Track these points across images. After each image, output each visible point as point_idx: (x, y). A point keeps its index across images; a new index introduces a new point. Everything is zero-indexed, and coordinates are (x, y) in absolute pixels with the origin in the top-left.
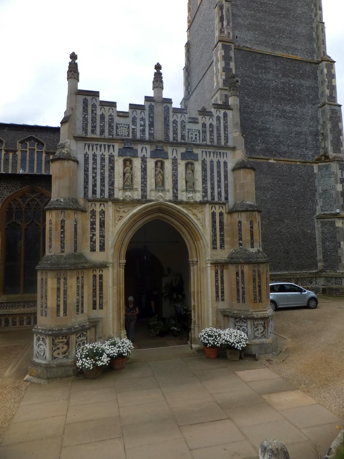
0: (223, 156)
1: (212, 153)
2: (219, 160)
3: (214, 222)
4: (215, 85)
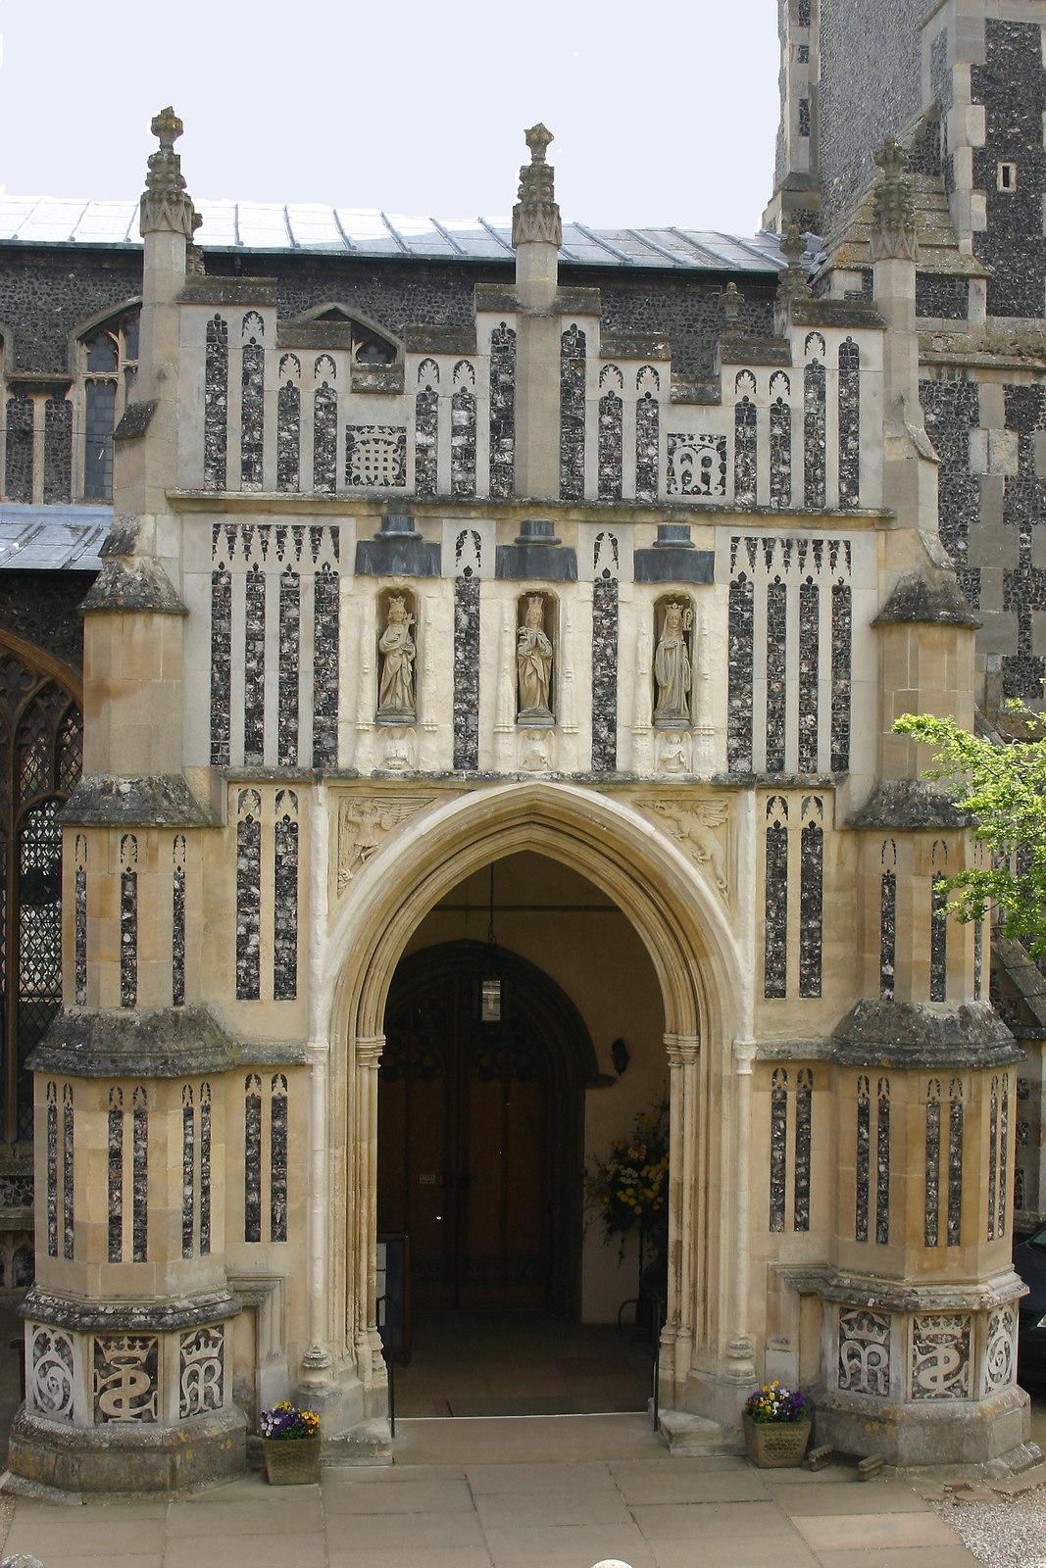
0: (834, 556)
1: (778, 545)
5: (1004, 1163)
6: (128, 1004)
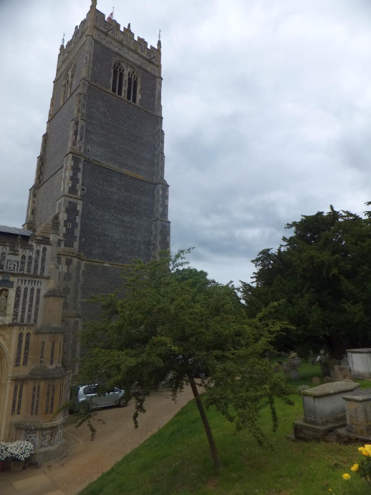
0: (38, 283)
1: (27, 281)
2: (33, 287)
3: (20, 342)
4: (62, 189)
5: (62, 396)
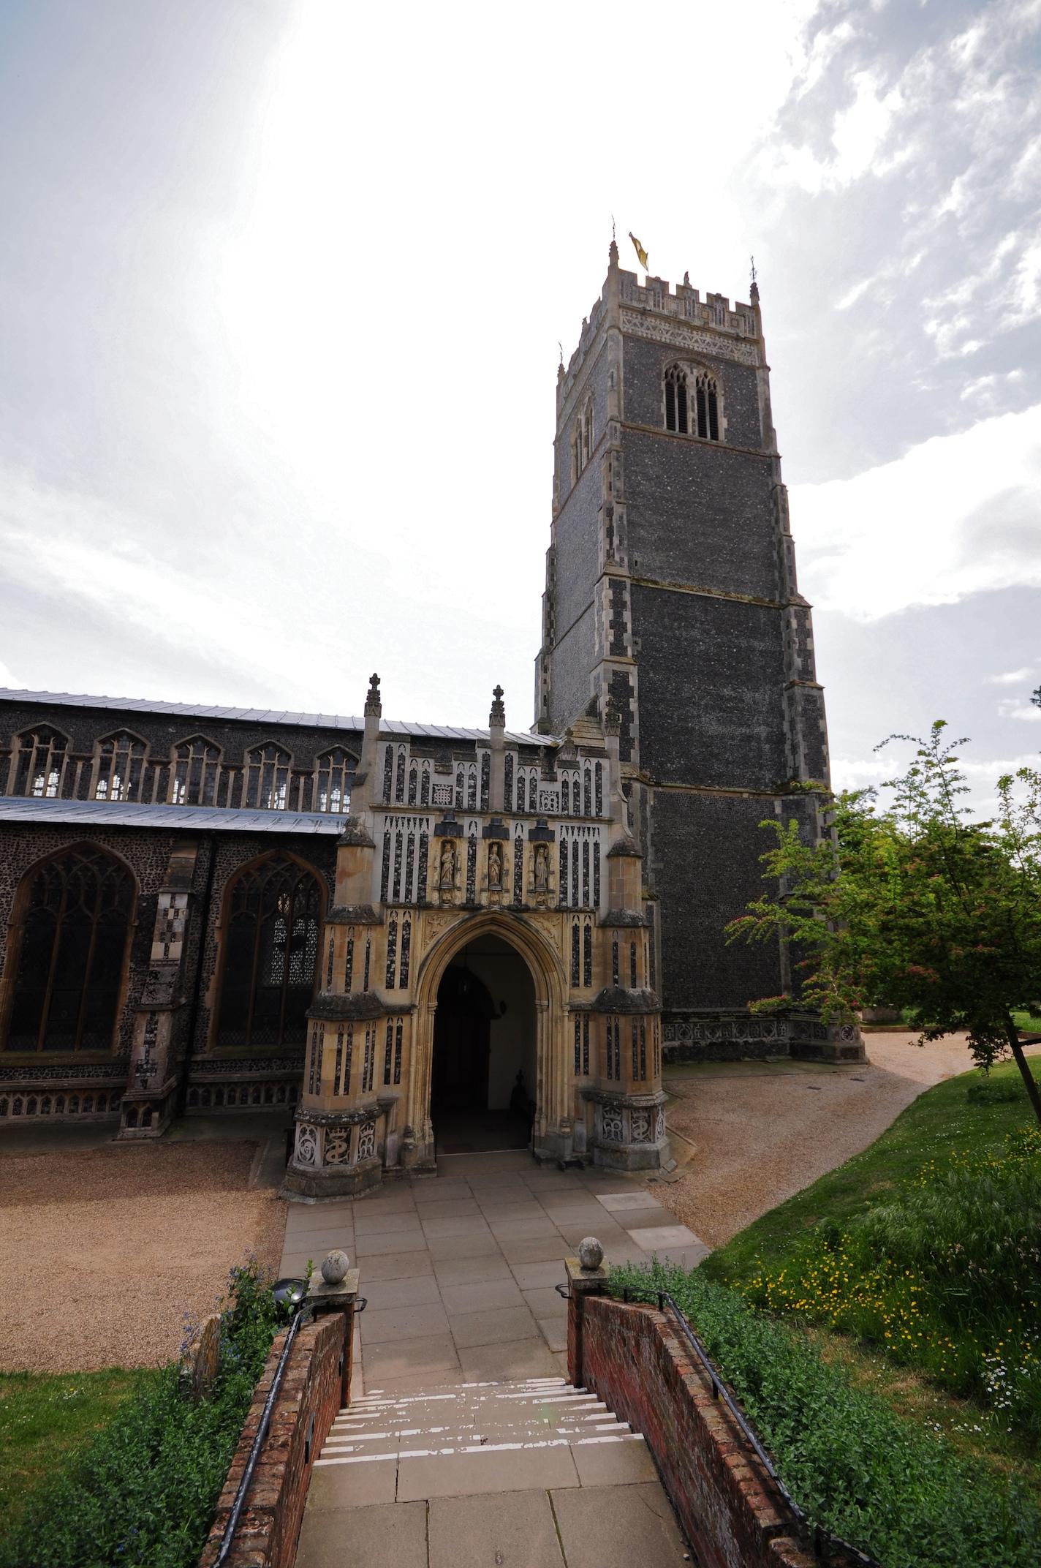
6: (347, 991)
